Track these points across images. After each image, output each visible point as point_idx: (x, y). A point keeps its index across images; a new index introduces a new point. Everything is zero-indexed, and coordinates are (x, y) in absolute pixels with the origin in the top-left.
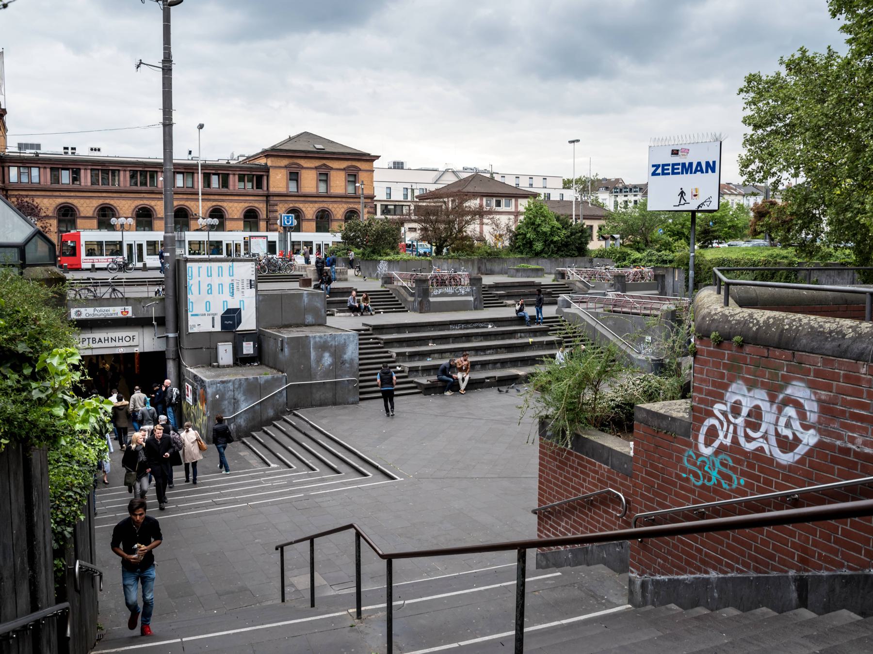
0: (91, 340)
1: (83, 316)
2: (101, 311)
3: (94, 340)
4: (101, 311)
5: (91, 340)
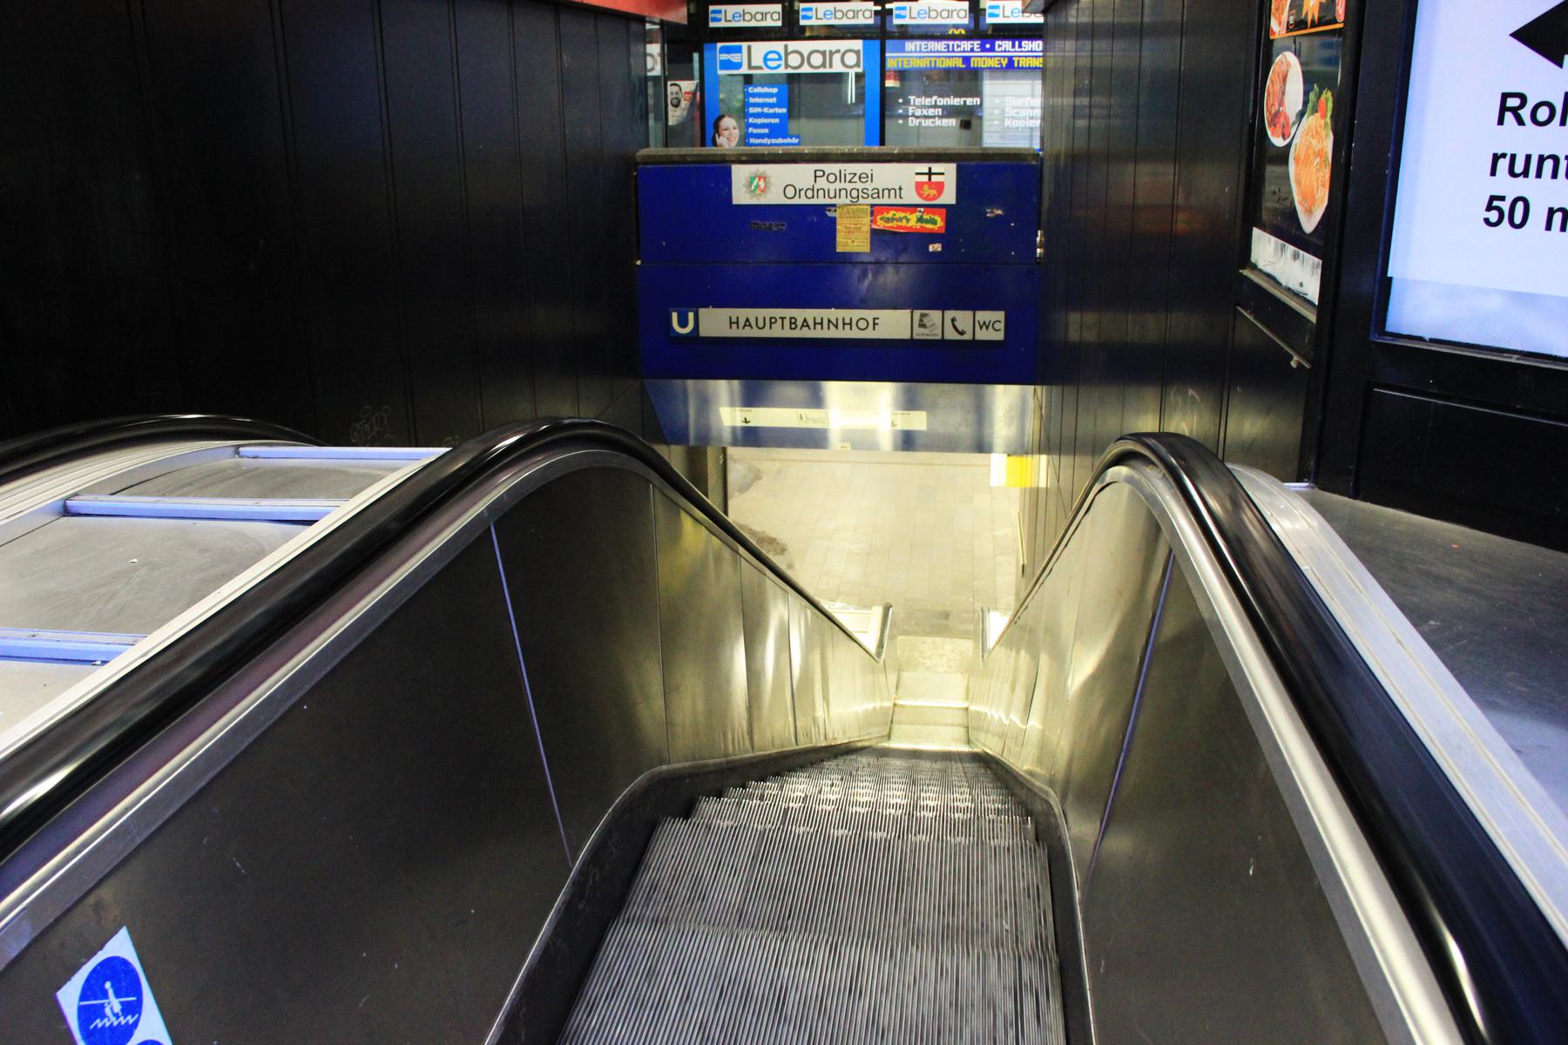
0: (787, 322)
1: (774, 197)
2: (840, 177)
3: (793, 321)
4: (840, 177)
5: (787, 322)
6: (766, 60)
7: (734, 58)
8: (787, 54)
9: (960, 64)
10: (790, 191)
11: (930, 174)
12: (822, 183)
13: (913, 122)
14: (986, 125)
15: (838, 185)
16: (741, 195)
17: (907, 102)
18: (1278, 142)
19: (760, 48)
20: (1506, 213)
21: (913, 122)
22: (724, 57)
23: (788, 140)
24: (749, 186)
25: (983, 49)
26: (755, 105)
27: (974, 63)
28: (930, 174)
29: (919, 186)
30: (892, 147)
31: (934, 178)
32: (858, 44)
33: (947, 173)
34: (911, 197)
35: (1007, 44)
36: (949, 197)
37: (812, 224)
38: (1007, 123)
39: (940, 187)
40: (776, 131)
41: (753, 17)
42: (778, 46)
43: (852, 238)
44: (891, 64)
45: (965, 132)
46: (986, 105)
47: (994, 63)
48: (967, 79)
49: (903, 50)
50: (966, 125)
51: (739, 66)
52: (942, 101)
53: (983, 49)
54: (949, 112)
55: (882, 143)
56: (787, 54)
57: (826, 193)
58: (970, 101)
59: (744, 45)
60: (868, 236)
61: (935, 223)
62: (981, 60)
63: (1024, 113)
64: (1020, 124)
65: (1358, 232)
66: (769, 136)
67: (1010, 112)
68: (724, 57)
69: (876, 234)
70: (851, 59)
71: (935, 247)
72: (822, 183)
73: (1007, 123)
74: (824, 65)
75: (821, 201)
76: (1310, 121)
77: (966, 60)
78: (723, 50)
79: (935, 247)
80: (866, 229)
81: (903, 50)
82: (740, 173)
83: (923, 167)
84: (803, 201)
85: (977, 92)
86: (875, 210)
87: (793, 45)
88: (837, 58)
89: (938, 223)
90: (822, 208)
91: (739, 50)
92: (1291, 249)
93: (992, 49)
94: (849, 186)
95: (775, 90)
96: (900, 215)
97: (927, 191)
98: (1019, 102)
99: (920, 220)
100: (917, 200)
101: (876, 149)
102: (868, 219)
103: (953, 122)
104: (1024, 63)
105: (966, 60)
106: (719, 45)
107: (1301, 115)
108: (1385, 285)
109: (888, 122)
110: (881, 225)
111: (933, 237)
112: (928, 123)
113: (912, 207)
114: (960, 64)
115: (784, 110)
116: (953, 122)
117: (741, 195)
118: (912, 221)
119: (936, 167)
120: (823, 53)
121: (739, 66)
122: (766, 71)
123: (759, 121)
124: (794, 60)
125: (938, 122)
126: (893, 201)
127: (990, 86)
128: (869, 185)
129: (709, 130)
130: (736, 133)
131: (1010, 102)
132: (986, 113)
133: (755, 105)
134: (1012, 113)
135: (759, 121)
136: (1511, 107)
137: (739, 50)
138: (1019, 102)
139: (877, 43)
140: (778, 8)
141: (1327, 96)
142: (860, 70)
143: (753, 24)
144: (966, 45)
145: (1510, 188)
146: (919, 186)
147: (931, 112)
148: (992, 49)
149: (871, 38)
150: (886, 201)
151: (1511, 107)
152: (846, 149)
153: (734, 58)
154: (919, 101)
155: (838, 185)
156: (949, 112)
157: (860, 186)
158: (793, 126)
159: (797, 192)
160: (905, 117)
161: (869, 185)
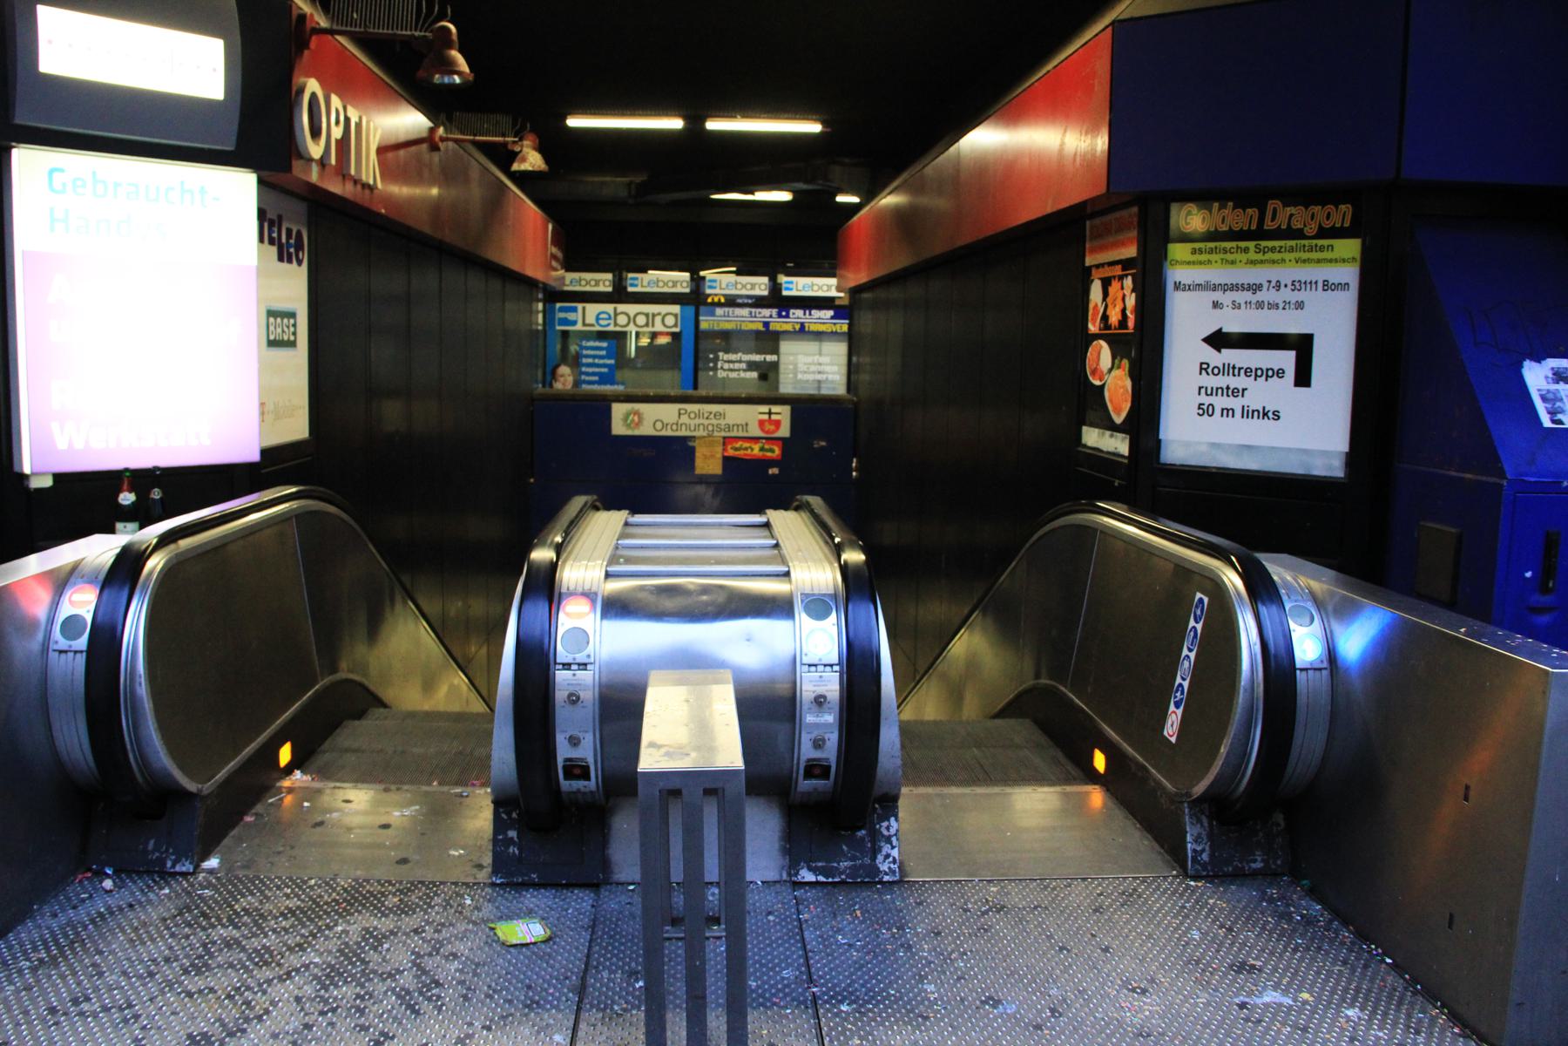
1: (646, 430)
2: (698, 415)
4: (698, 415)
6: (598, 319)
7: (571, 316)
8: (616, 314)
9: (761, 327)
10: (659, 426)
11: (770, 413)
12: (684, 419)
13: (721, 374)
14: (782, 377)
15: (697, 421)
16: (618, 428)
17: (716, 359)
18: (1097, 383)
19: (593, 309)
20: (1205, 411)
21: (721, 374)
22: (562, 315)
23: (615, 387)
24: (622, 421)
25: (780, 316)
26: (587, 356)
27: (772, 327)
28: (770, 413)
29: (761, 423)
30: (702, 392)
31: (774, 417)
32: (676, 309)
33: (783, 413)
34: (755, 431)
35: (799, 313)
36: (785, 431)
37: (677, 450)
38: (800, 376)
39: (778, 424)
40: (604, 379)
41: (588, 283)
42: (609, 308)
43: (708, 463)
44: (704, 326)
45: (763, 384)
46: (783, 359)
47: (789, 327)
48: (768, 339)
49: (713, 314)
50: (763, 377)
51: (574, 323)
52: (747, 357)
53: (780, 316)
54: (752, 366)
55: (696, 387)
56: (616, 314)
57: (688, 427)
58: (770, 358)
59: (580, 306)
60: (720, 462)
61: (772, 451)
62: (778, 325)
63: (813, 368)
64: (810, 377)
65: (1144, 418)
66: (599, 383)
67: (801, 367)
68: (562, 315)
69: (727, 461)
70: (670, 321)
71: (774, 471)
72: (684, 419)
73: (800, 376)
74: (647, 325)
75: (683, 433)
76: (1116, 373)
77: (766, 324)
78: (562, 310)
79: (774, 471)
80: (719, 455)
81: (713, 314)
82: (619, 410)
83: (765, 408)
84: (669, 433)
85: (776, 351)
86: (727, 441)
87: (621, 307)
88: (658, 320)
89: (776, 452)
90: (685, 439)
91: (575, 310)
92: (1108, 433)
93: (787, 316)
94: (706, 422)
95: (605, 344)
96: (746, 445)
97: (768, 427)
98: (810, 359)
99: (762, 449)
100: (759, 433)
101: (690, 392)
102: (720, 449)
103: (755, 375)
104: (814, 328)
105: (766, 324)
106: (558, 305)
107: (1110, 370)
108: (1158, 443)
109: (701, 374)
110: (731, 452)
111: (771, 463)
112: (733, 375)
113: (756, 439)
114: (761, 327)
115: (612, 362)
116: (755, 375)
117: (618, 428)
118: (756, 450)
119: (775, 409)
120: (647, 315)
121: (574, 323)
122: (598, 328)
123: (590, 370)
124: (622, 320)
125: (742, 374)
126: (741, 434)
127: (785, 346)
128: (722, 422)
129: (548, 378)
130: (571, 379)
131: (802, 360)
132: (782, 367)
133: (587, 356)
134: (804, 368)
135: (590, 370)
136: (1204, 368)
137: (575, 310)
138: (810, 359)
139: (691, 310)
140: (609, 276)
141: (1126, 363)
142: (677, 330)
143: (588, 289)
144: (766, 312)
145: (1207, 400)
146: (761, 423)
147: (737, 366)
148: (787, 316)
149: (688, 304)
150: (734, 434)
151: (1204, 368)
152: (661, 391)
153: (571, 316)
154: (726, 357)
155: (697, 421)
156: (752, 366)
157: (715, 422)
158: (618, 375)
159: (665, 426)
160: (715, 369)
161: (722, 422)
